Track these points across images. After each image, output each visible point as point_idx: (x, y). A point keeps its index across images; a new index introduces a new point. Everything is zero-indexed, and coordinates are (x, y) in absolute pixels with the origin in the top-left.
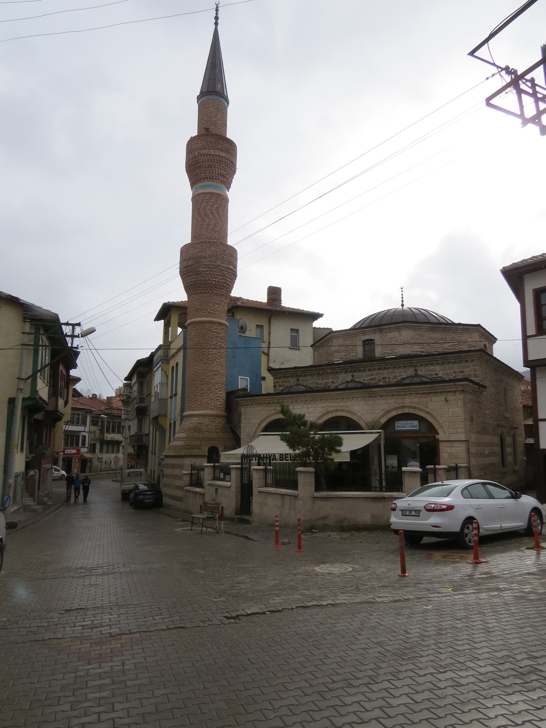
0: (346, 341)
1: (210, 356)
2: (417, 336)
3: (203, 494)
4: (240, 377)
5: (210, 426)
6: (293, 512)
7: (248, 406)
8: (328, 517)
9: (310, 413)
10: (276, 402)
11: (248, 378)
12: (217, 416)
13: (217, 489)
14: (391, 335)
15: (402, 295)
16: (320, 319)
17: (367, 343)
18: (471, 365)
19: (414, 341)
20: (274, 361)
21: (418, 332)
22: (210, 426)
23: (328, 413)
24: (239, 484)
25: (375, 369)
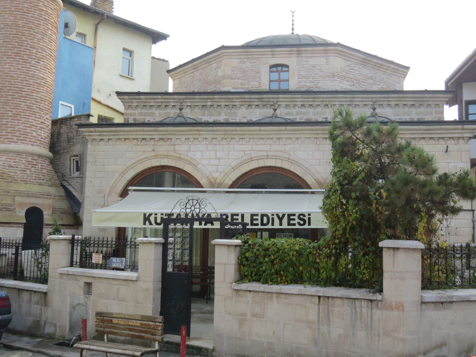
0: (244, 63)
1: (34, 51)
2: (347, 68)
3: (45, 294)
4: (61, 102)
5: (28, 172)
6: (361, 334)
7: (102, 143)
8: (445, 344)
9: (219, 159)
10: (157, 137)
11: (73, 107)
12: (39, 156)
13: (89, 285)
14: (312, 61)
15: (293, 21)
16: (161, 44)
17: (274, 69)
18: (434, 111)
19: (344, 74)
20: (98, 91)
21: (349, 63)
22: (28, 172)
23: (252, 160)
24: (159, 274)
25: (295, 105)
